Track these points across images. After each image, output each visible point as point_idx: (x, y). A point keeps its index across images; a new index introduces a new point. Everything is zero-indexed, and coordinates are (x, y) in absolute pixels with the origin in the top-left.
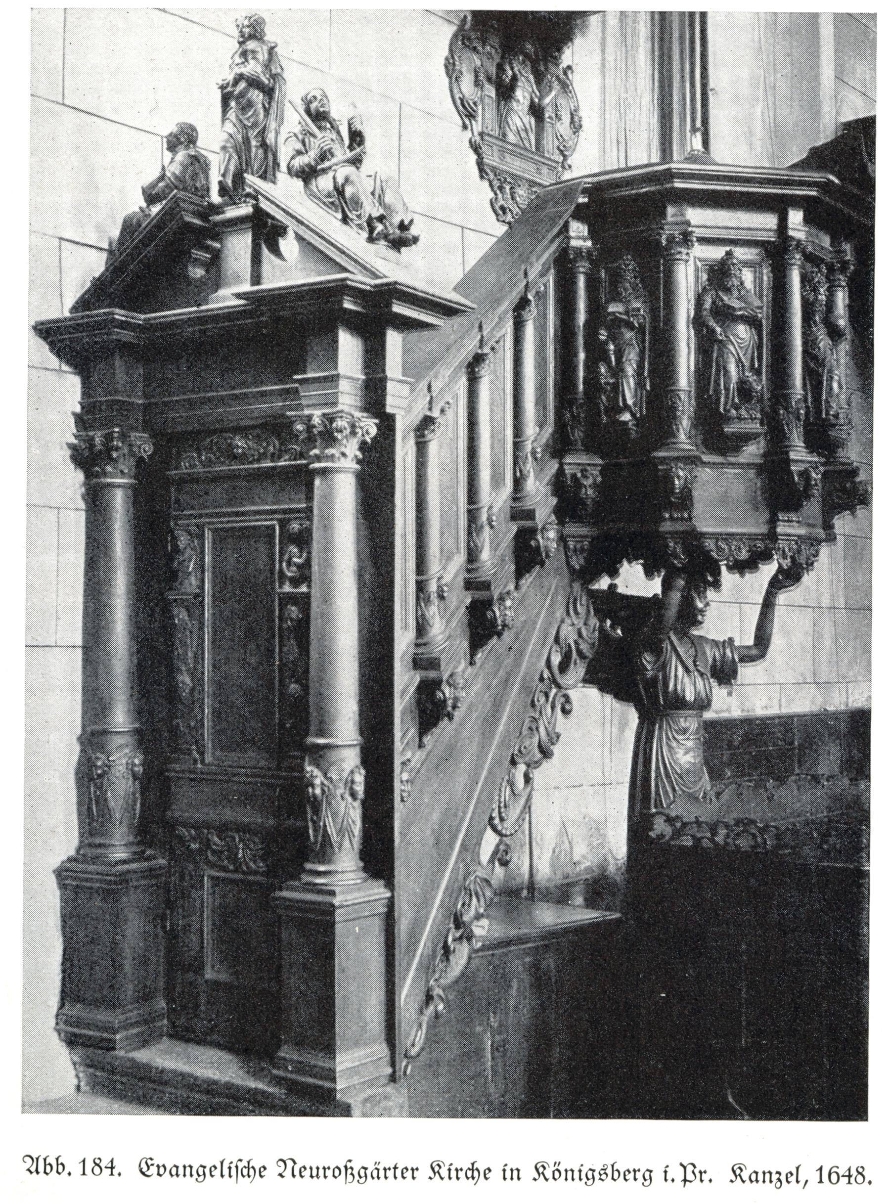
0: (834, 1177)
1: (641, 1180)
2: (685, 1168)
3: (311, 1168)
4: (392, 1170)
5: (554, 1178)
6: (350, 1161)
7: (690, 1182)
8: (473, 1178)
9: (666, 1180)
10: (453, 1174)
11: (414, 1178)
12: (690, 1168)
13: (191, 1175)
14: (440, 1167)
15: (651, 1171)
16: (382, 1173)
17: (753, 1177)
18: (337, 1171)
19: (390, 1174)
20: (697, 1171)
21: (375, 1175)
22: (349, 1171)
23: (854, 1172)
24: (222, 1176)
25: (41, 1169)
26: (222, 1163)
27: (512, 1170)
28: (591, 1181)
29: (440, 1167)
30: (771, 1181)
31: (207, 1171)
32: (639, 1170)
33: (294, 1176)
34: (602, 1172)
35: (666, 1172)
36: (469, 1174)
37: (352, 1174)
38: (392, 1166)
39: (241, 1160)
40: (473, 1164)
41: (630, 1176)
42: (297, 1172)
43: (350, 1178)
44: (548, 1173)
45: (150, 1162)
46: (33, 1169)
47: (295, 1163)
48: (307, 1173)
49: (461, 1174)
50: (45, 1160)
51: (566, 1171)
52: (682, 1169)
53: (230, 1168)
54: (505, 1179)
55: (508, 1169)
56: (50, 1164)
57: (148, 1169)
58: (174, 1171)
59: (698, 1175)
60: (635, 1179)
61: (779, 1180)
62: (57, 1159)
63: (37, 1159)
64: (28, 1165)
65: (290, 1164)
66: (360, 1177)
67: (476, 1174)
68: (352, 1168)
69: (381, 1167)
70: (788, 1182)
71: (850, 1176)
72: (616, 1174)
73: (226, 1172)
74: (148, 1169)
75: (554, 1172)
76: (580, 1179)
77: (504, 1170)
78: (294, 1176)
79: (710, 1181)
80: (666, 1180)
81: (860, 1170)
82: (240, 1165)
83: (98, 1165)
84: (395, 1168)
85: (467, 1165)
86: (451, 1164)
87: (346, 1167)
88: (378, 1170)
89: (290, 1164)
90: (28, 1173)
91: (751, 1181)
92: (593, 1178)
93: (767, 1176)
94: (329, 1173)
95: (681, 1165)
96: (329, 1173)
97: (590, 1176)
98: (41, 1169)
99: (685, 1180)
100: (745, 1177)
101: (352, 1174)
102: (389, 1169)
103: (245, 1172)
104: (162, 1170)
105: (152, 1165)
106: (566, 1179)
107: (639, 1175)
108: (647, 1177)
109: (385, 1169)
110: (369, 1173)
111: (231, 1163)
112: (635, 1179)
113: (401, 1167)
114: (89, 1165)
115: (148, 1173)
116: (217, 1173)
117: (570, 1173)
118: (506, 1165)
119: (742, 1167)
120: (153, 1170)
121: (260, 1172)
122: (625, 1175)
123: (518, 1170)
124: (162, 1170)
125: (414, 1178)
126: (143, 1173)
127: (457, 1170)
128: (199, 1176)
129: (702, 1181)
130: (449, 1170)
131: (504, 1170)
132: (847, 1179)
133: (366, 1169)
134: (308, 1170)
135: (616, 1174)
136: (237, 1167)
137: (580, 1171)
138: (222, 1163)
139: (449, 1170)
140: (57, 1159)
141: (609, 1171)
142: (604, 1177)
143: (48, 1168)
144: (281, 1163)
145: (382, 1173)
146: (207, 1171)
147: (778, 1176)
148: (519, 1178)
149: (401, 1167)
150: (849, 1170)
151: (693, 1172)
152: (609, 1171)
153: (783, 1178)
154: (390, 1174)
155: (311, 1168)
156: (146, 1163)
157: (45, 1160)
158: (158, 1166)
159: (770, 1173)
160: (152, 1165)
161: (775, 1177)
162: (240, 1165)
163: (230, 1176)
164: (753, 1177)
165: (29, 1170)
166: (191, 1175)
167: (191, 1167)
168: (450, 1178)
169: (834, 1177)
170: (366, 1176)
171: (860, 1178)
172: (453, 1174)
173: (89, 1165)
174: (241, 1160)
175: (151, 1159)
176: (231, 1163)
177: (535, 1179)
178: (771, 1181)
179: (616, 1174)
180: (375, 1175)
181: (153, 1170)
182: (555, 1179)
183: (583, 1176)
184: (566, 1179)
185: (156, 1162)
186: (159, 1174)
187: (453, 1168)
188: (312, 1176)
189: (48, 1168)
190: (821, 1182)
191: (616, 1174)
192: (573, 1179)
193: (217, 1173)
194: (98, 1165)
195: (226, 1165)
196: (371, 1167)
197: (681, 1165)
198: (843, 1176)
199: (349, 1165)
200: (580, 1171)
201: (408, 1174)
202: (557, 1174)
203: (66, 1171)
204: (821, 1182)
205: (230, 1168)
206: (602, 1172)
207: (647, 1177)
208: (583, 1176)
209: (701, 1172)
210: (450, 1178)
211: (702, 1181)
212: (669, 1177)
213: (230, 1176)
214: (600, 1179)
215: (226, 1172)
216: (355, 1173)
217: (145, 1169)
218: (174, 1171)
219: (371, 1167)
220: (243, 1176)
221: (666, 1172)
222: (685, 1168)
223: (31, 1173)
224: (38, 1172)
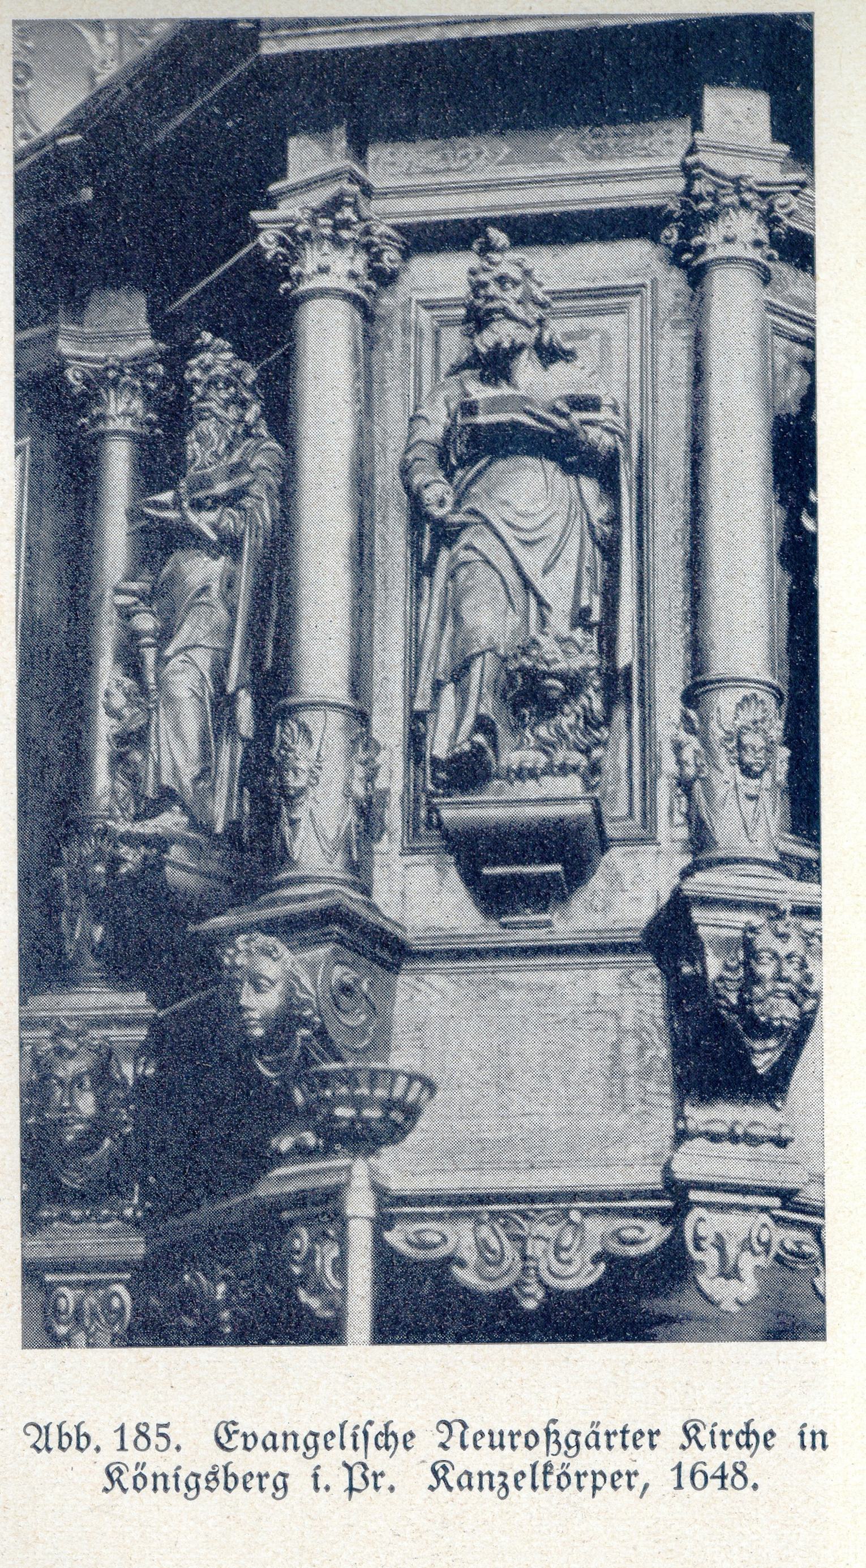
0: (699, 1478)
1: (270, 1489)
2: (350, 1469)
3: (491, 1434)
4: (620, 1435)
5: (135, 1487)
6: (554, 1421)
7: (359, 1491)
8: (748, 1446)
9: (316, 1488)
10: (718, 1440)
11: (652, 1446)
12: (357, 1472)
13: (296, 1448)
14: (698, 1429)
15: (284, 1475)
16: (603, 1440)
17: (464, 1481)
18: (532, 1440)
19: (616, 1441)
20: (368, 1474)
21: (592, 1442)
22: (553, 1437)
23: (729, 1471)
24: (343, 1447)
25: (53, 1443)
26: (342, 1427)
27: (813, 1434)
28: (573, 1451)
29: (698, 1429)
30: (491, 1488)
31: (320, 1441)
32: (267, 1475)
33: (463, 1446)
34: (211, 1477)
35: (316, 1476)
36: (743, 1439)
37: (557, 1442)
38: (619, 1429)
39: (370, 1423)
40: (748, 1425)
41: (254, 1483)
42: (469, 1440)
43: (554, 1448)
44: (127, 1481)
45: (231, 1428)
46: (41, 1444)
47: (465, 1426)
48: (484, 1442)
49: (731, 1440)
50: (60, 1428)
51: (155, 1476)
52: (346, 1471)
53: (355, 1436)
54: (803, 1446)
55: (807, 1431)
56: (67, 1434)
57: (230, 1438)
58: (269, 1443)
59: (371, 1480)
60: (262, 1489)
61: (504, 1485)
62: (78, 1428)
63: (47, 1428)
64: (32, 1440)
65: (457, 1428)
66: (569, 1447)
67: (753, 1439)
68: (556, 1433)
69: (602, 1430)
70: (519, 1488)
71: (723, 1477)
72: (231, 1481)
73: (348, 1442)
74: (230, 1438)
75: (135, 1478)
76: (177, 1489)
77: (802, 1434)
78: (463, 1446)
79: (392, 1489)
80: (316, 1488)
81: (740, 1467)
82: (372, 1431)
83: (144, 1434)
84: (624, 1432)
85: (738, 1427)
86: (715, 1424)
87: (547, 1432)
88: (597, 1434)
89: (457, 1428)
90: (34, 1450)
91: (740, 1446)
92: (197, 1486)
93: (486, 1479)
94: (519, 1441)
95: (345, 1465)
96: (519, 1441)
97: (192, 1485)
98: (53, 1443)
99: (351, 1489)
100: (452, 1481)
101: (557, 1442)
102: (615, 1433)
103: (381, 1441)
104: (251, 1441)
105: (236, 1432)
106: (155, 1489)
107: (267, 1483)
108: (280, 1484)
109: (608, 1434)
110: (582, 1440)
111: (357, 1427)
112: (262, 1489)
113: (632, 1429)
114: (130, 1434)
115: (228, 1446)
116: (335, 1442)
117: (160, 1481)
118: (804, 1425)
119: (448, 1466)
120: (237, 1440)
121: (405, 1442)
122: (245, 1483)
123: (823, 1434)
124: (251, 1441)
125: (652, 1446)
126: (222, 1446)
127: (723, 1434)
128: (308, 1448)
129: (376, 1488)
130: (712, 1433)
131: (802, 1434)
132: (719, 1481)
133: (577, 1434)
134: (487, 1437)
135: (231, 1480)
136: (366, 1434)
137: (176, 1476)
138: (342, 1427)
139: (712, 1433)
140: (78, 1428)
141: (221, 1475)
142: (213, 1484)
143: (65, 1440)
144: (443, 1428)
145: (603, 1440)
146: (320, 1441)
147: (502, 1478)
148: (824, 1446)
149: (632, 1429)
150: (723, 1467)
151: (364, 1477)
152: (221, 1475)
153: (510, 1482)
154: (616, 1441)
155: (491, 1434)
156: (227, 1430)
157: (60, 1428)
158: (245, 1436)
159: (491, 1475)
160: (236, 1432)
161: (497, 1480)
162: (372, 1431)
163: (355, 1448)
164: (464, 1481)
165: (34, 1446)
166: (296, 1448)
167: (295, 1435)
168: (714, 1446)
169: (699, 1478)
170: (578, 1445)
171: (739, 1481)
172: (718, 1440)
173: (130, 1434)
174: (370, 1423)
175: (234, 1423)
176: (357, 1427)
177: (106, 1490)
178: (491, 1488)
179: (231, 1480)
180: (592, 1442)
181: (237, 1440)
182: (138, 1490)
183: (182, 1485)
184: (155, 1489)
185: (242, 1428)
186: (246, 1448)
187: (717, 1430)
188: (492, 1446)
189: (65, 1440)
190: (679, 1486)
191: (231, 1481)
192: (166, 1489)
193: (335, 1442)
194: (144, 1434)
195: (348, 1432)
196: (585, 1430)
197: (345, 1465)
198: (713, 1477)
199: (552, 1428)
200: (176, 1476)
201: (645, 1441)
202: (140, 1482)
203: (92, 1446)
204: (679, 1486)
205: (355, 1436)
206: (211, 1477)
207: (280, 1484)
208: (182, 1485)
209: (375, 1475)
210: (714, 1446)
211: (376, 1488)
212: (321, 1484)
213: (355, 1448)
214: (208, 1488)
215: (348, 1442)
216: (562, 1440)
217: (224, 1439)
218: (269, 1443)
219: (585, 1430)
220: (378, 1447)
221: (316, 1476)
222: (350, 1469)
223: (39, 1450)
224: (49, 1449)
